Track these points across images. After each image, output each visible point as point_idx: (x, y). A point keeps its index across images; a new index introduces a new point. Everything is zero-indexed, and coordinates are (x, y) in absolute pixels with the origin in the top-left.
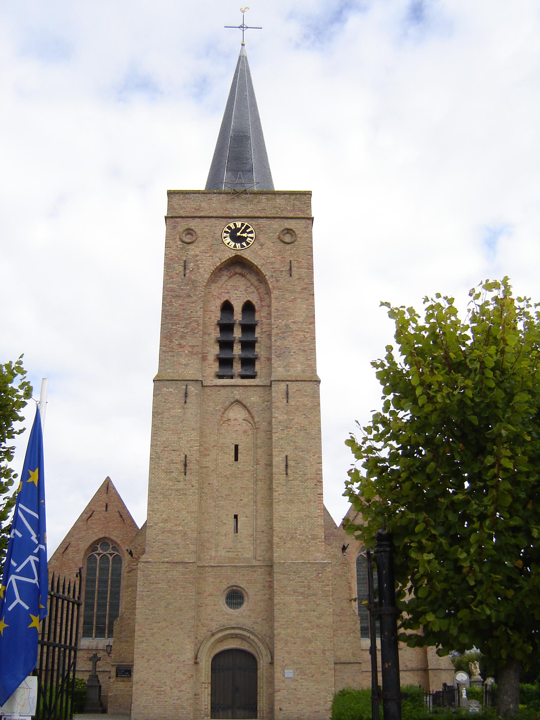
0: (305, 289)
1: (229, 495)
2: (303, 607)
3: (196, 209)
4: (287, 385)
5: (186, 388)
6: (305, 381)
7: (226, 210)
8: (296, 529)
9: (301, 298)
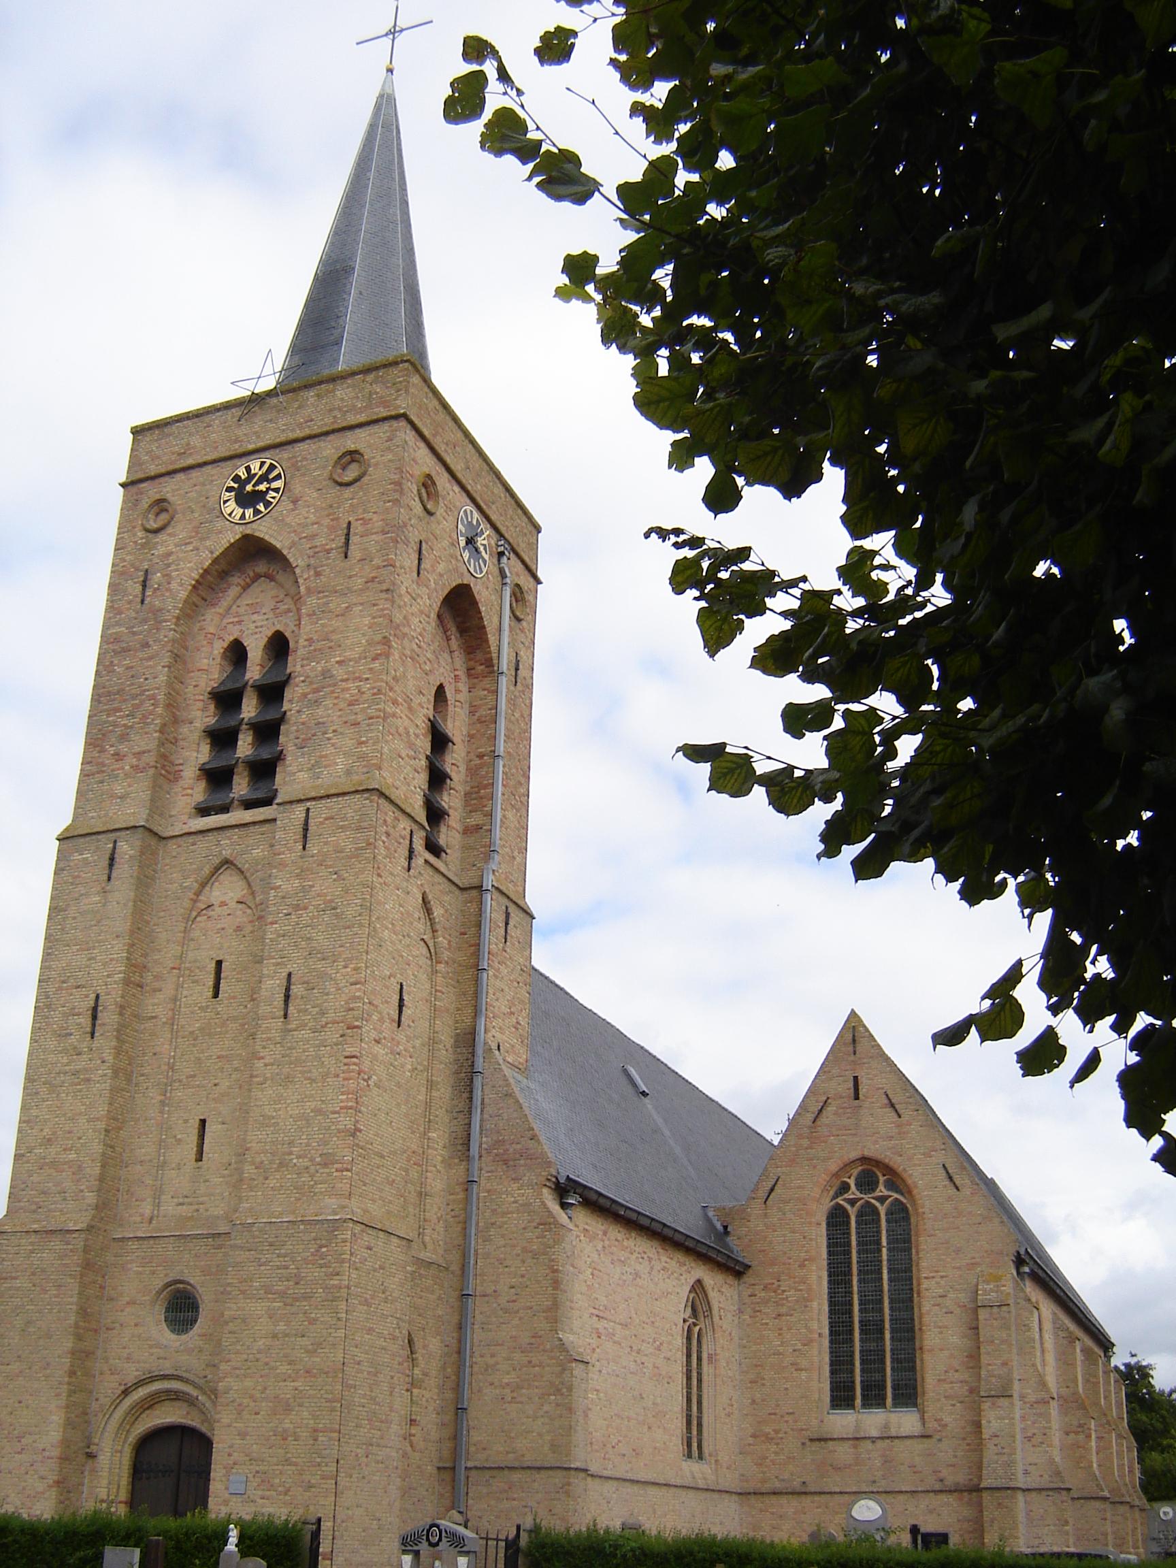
0: (373, 580)
1: (194, 1076)
2: (282, 1327)
3: (179, 454)
4: (308, 810)
5: (114, 848)
6: (344, 794)
7: (236, 441)
8: (291, 1143)
9: (361, 604)
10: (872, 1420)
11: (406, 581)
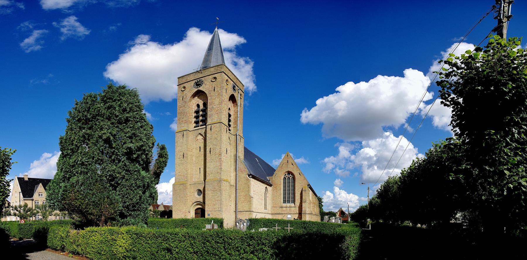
10: (288, 205)
11: (224, 94)
